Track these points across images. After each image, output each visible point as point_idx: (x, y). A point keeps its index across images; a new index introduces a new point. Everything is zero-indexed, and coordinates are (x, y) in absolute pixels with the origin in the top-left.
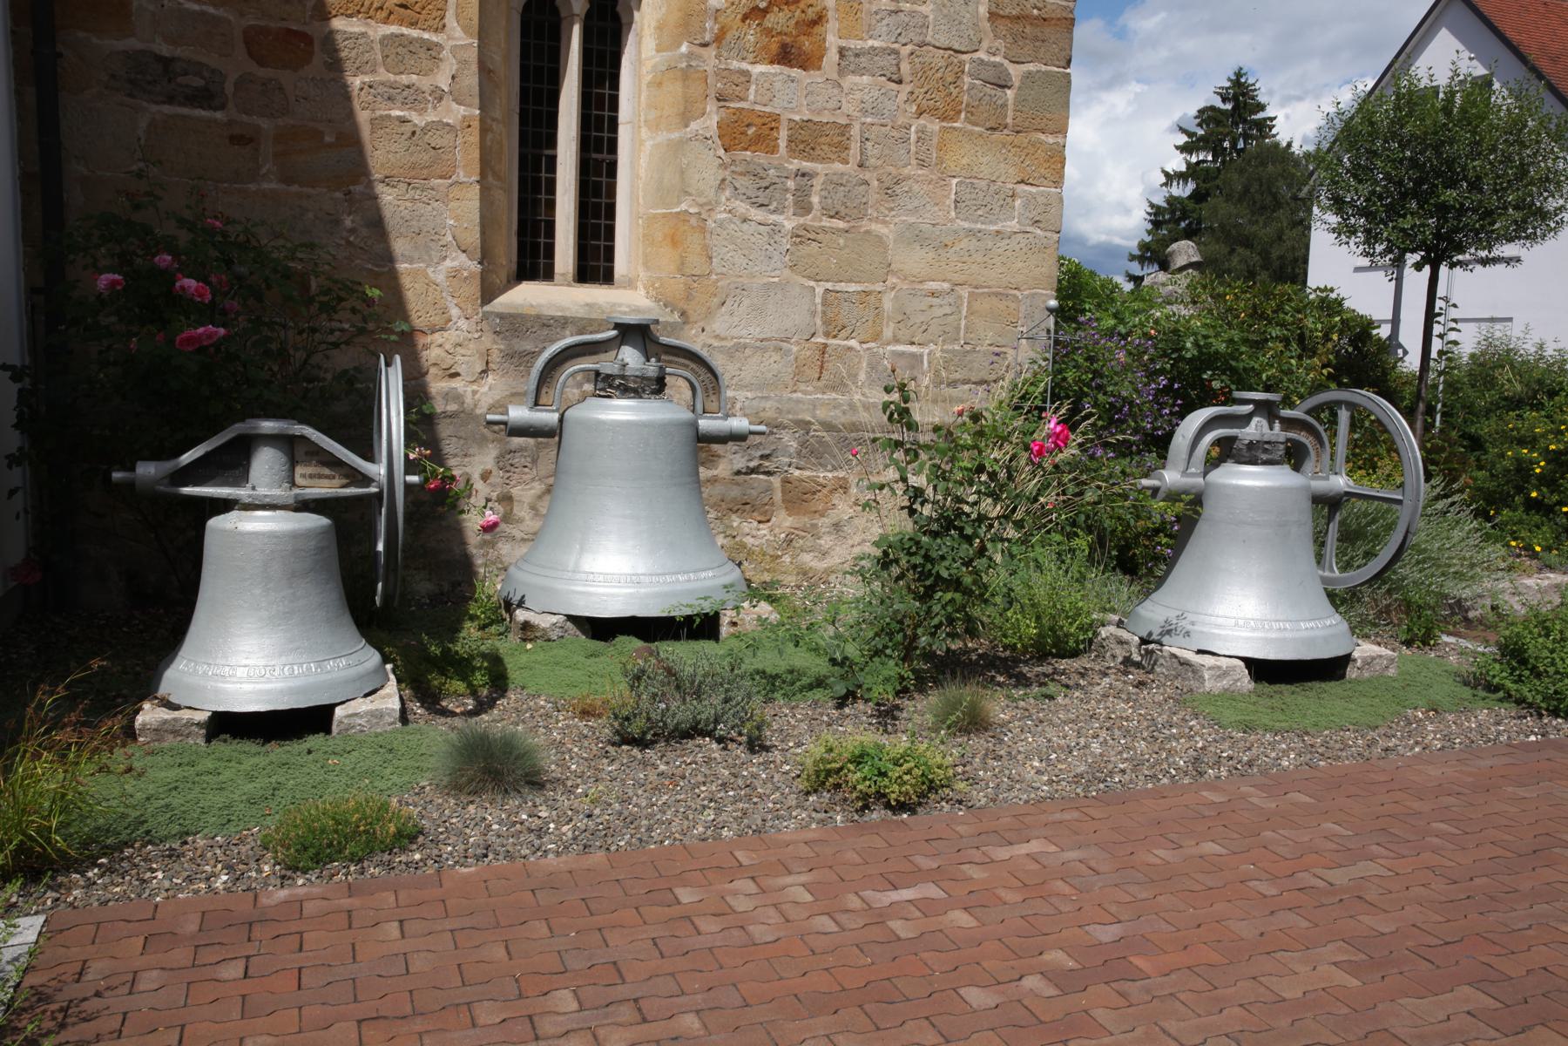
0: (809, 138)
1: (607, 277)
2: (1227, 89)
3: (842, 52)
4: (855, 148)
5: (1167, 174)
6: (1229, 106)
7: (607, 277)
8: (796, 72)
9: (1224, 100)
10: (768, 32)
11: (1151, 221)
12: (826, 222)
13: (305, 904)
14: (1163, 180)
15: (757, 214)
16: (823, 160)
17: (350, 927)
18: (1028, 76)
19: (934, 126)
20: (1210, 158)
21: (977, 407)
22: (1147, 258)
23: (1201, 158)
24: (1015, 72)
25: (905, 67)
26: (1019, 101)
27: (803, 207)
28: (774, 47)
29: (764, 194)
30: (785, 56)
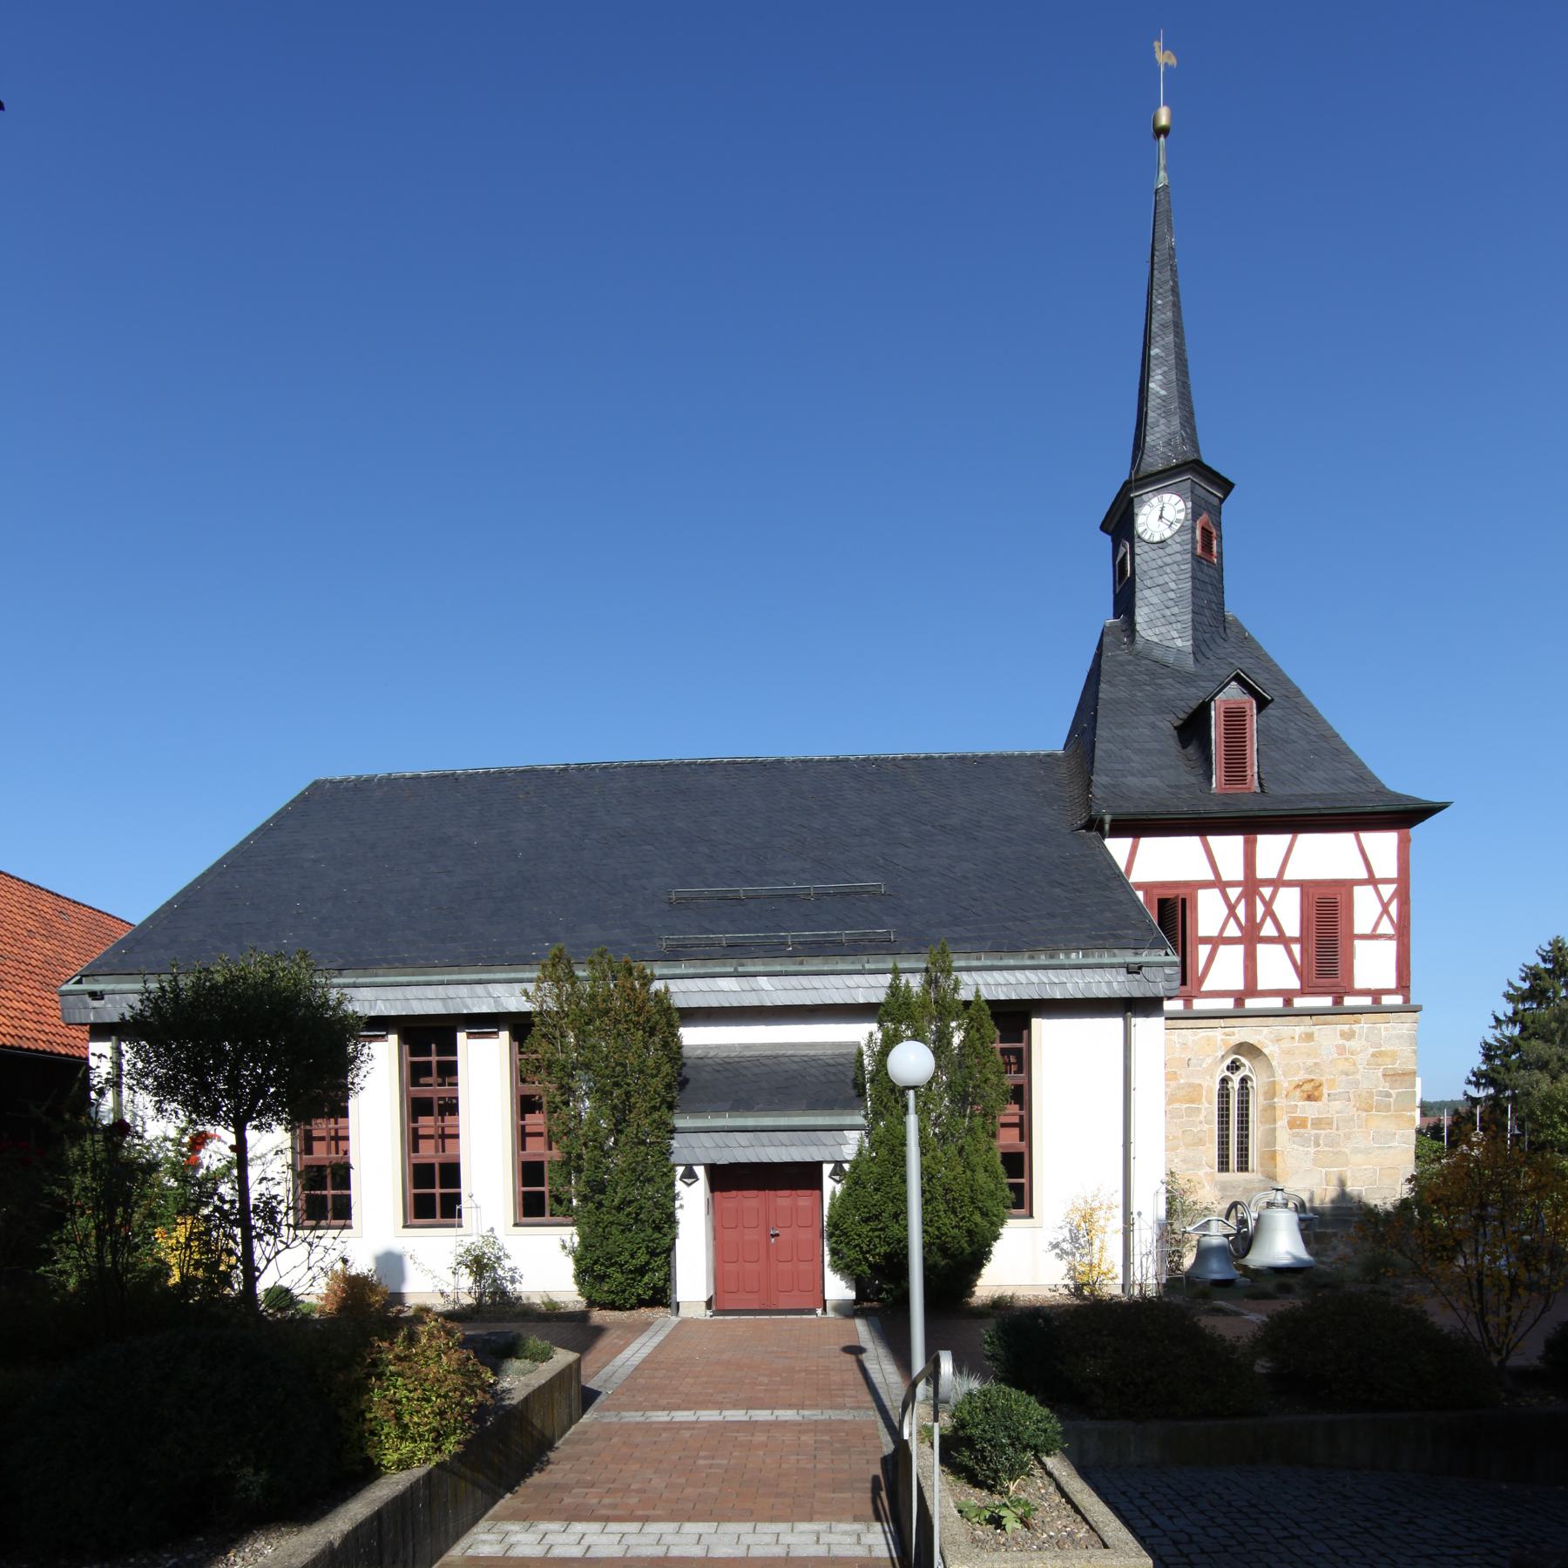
0: (1318, 1123)
1: (1246, 1169)
2: (1547, 952)
3: (1329, 1095)
4: (1335, 1125)
5: (1497, 1019)
6: (1549, 966)
7: (1246, 1169)
8: (1313, 1103)
9: (1544, 960)
10: (1303, 1091)
11: (1484, 1055)
12: (1325, 1149)
13: (672, 1547)
14: (1494, 1024)
15: (1301, 1148)
16: (1323, 1129)
17: (777, 1543)
18: (1398, 1094)
19: (1364, 1114)
20: (1535, 1006)
21: (1302, 1076)
22: (1482, 1084)
23: (1527, 1006)
24: (1393, 1092)
25: (1351, 1096)
26: (1395, 1101)
27: (1317, 1144)
28: (1305, 1096)
29: (1305, 1142)
30: (1309, 1098)
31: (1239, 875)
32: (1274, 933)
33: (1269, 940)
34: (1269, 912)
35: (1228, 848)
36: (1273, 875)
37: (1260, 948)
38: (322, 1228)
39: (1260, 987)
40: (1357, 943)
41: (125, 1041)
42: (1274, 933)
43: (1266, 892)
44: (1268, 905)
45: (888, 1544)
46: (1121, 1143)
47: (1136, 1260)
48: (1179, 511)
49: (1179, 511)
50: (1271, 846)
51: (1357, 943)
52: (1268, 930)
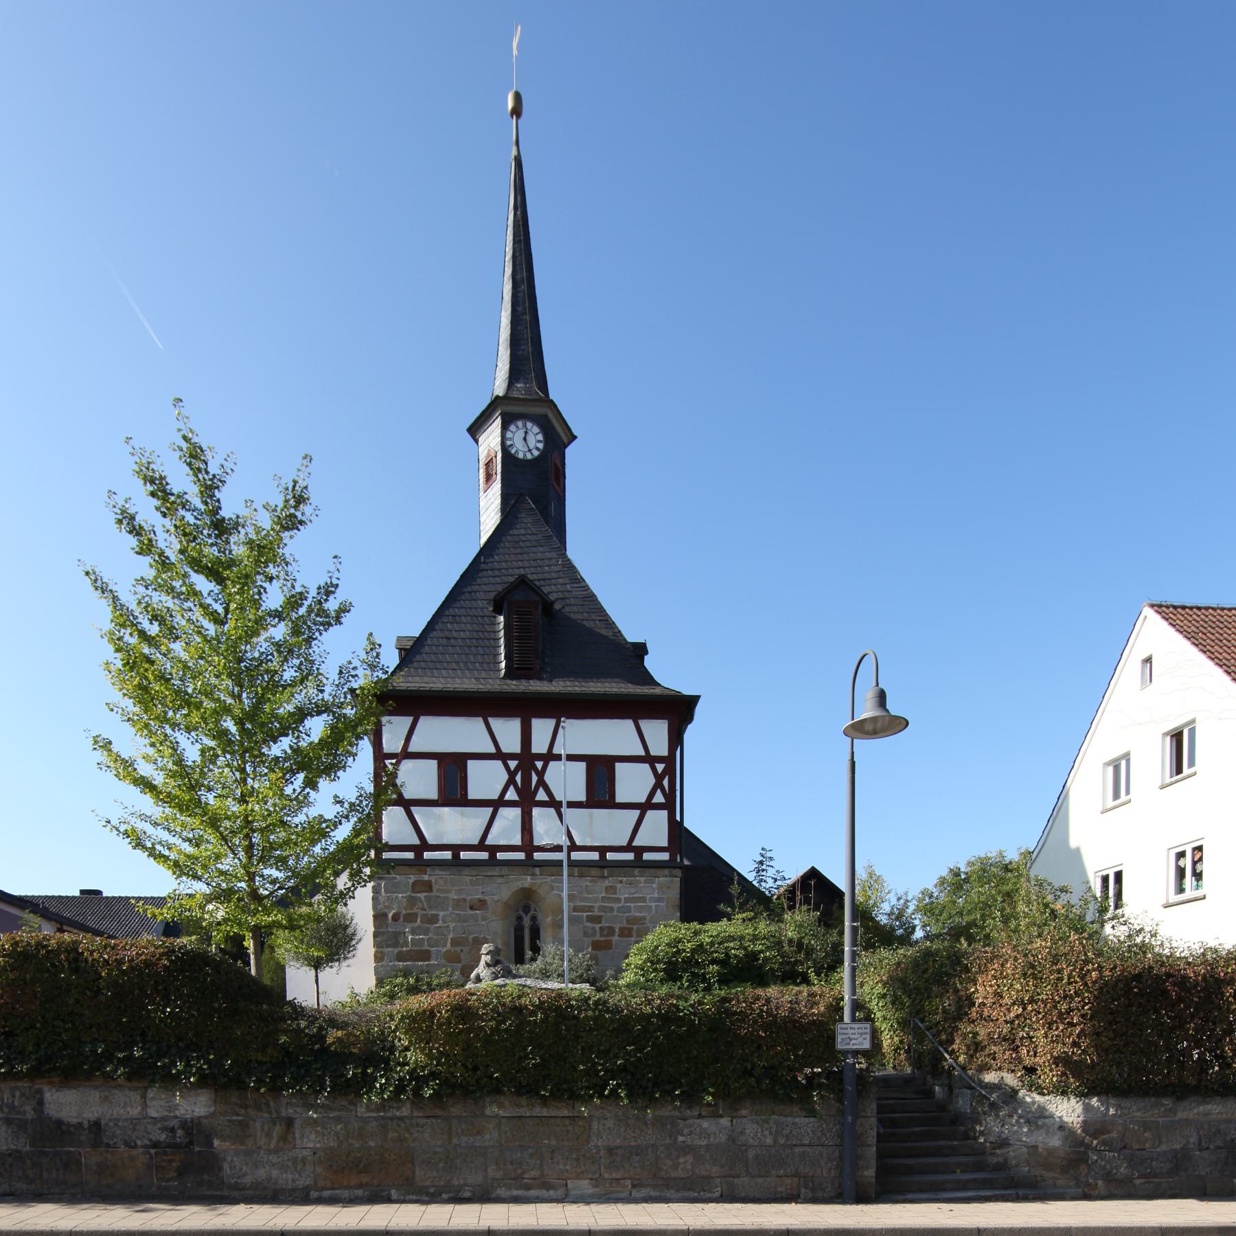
31: (516, 748)
32: (546, 798)
33: (542, 804)
34: (542, 783)
35: (508, 732)
36: (544, 750)
37: (536, 811)
38: (352, 951)
39: (582, 766)
40: (665, 843)
41: (321, 777)
42: (546, 798)
43: (539, 764)
44: (541, 774)
45: (1098, 724)
46: (559, 407)
47: (858, 888)
48: (517, 427)
49: (517, 427)
50: (542, 729)
51: (665, 843)
52: (541, 796)
